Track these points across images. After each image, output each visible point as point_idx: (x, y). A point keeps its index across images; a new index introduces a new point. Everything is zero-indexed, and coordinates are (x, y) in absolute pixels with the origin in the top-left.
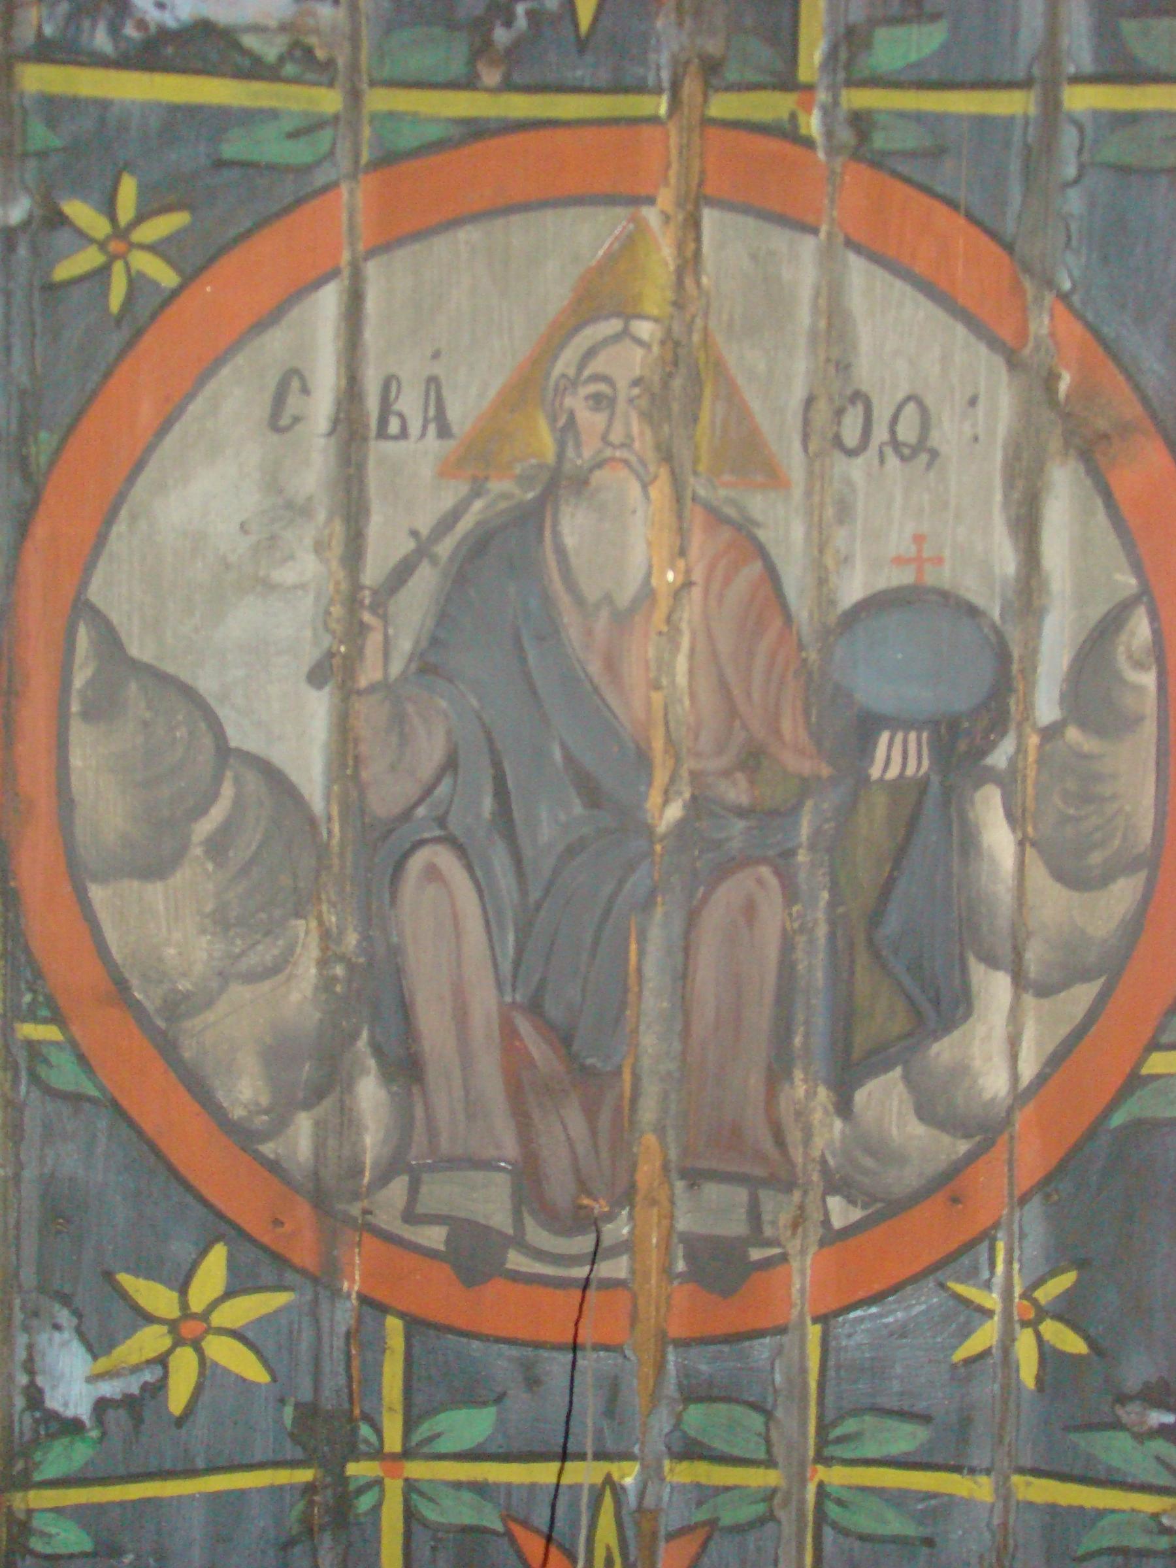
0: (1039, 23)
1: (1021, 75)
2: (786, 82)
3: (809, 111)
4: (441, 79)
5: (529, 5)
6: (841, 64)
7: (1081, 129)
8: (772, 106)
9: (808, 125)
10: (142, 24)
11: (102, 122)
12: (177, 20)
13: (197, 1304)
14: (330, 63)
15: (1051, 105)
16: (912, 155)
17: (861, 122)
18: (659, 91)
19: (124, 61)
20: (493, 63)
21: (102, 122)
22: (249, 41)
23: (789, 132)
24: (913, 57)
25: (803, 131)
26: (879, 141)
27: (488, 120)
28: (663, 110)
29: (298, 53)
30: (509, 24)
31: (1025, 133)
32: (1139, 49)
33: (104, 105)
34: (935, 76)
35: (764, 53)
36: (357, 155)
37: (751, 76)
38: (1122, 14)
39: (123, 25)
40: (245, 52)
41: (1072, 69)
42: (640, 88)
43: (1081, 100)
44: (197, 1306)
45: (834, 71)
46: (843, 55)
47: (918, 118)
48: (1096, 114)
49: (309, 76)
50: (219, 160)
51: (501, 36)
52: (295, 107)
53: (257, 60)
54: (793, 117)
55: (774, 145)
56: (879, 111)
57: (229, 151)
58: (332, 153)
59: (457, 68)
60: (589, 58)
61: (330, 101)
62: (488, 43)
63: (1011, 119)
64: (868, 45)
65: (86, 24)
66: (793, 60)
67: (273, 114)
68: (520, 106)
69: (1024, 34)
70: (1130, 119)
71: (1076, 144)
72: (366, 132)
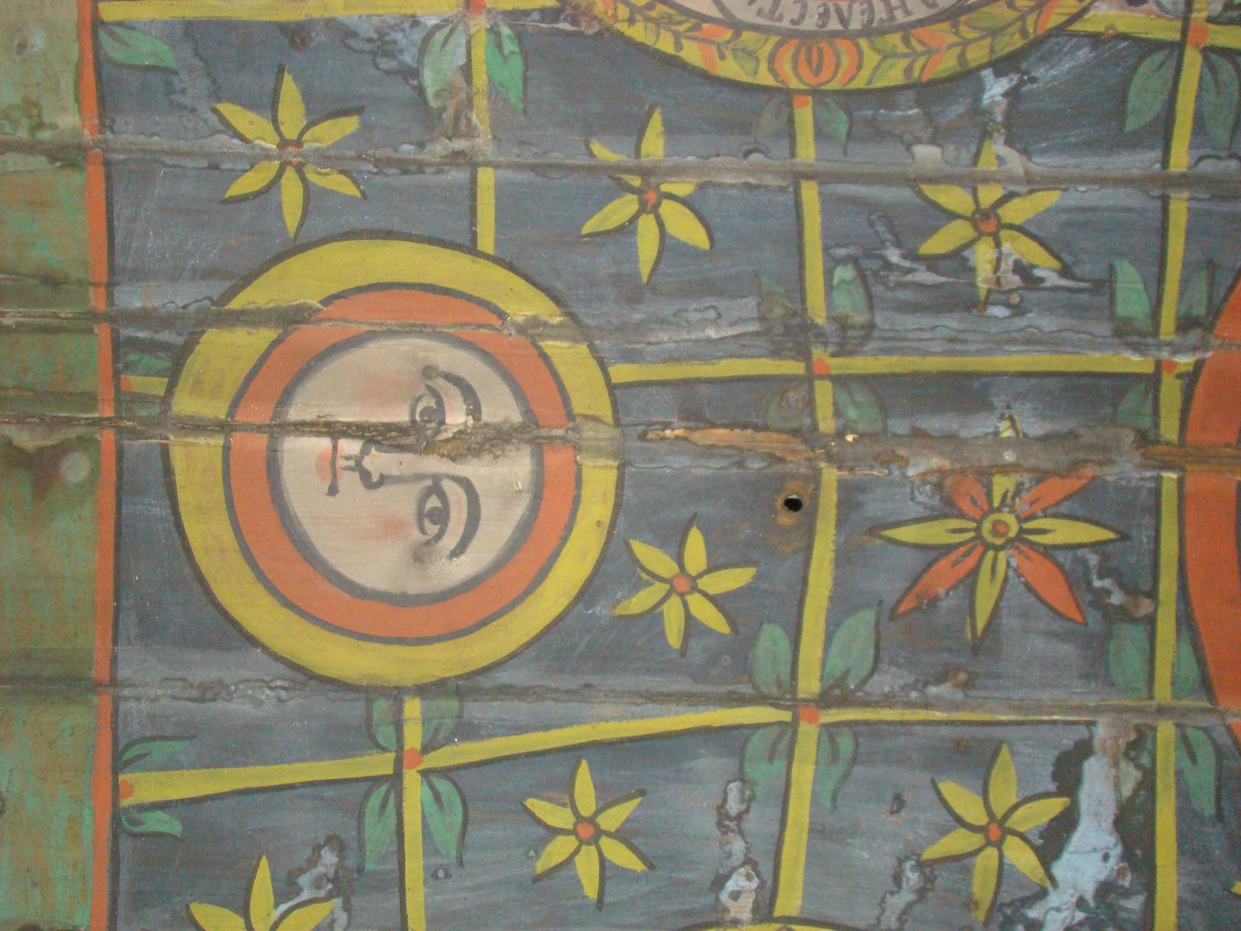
1: (1159, 204)
2: (1153, 381)
3: (1175, 365)
4: (1146, 645)
5: (1094, 577)
6: (1142, 340)
7: (1201, 159)
8: (1171, 391)
9: (1184, 365)
10: (1121, 873)
11: (1194, 906)
12: (1115, 845)
13: (605, 842)
14: (1138, 729)
15: (1182, 181)
16: (1212, 285)
17: (1186, 324)
18: (1158, 479)
19: (1150, 888)
20: (1136, 606)
21: (1194, 906)
22: (1127, 790)
23: (1191, 379)
24: (1140, 286)
25: (1191, 369)
26: (1200, 311)
27: (1178, 611)
28: (1173, 475)
29: (1133, 754)
30: (1108, 593)
32: (1148, 117)
33: (1181, 903)
34: (1155, 269)
35: (1131, 400)
36: (1204, 711)
37: (1148, 409)
38: (1121, 130)
39: (1122, 887)
40: (1135, 792)
41: (1158, 166)
42: (1157, 492)
43: (1180, 159)
45: (1146, 345)
46: (1135, 339)
47: (1185, 281)
49: (1149, 745)
50: (1217, 816)
51: (1116, 598)
52: (1172, 758)
53: (1140, 785)
54: (1179, 376)
55: (1200, 389)
56: (1178, 311)
57: (1209, 810)
58: (1205, 730)
59: (1139, 632)
60: (1134, 532)
61: (1166, 731)
62: (1121, 607)
63: (1189, 210)
64: (1128, 321)
65: (1122, 914)
66: (1138, 377)
67: (1179, 773)
68: (1168, 585)
69: (1129, 203)
71: (1210, 161)
72: (1187, 702)
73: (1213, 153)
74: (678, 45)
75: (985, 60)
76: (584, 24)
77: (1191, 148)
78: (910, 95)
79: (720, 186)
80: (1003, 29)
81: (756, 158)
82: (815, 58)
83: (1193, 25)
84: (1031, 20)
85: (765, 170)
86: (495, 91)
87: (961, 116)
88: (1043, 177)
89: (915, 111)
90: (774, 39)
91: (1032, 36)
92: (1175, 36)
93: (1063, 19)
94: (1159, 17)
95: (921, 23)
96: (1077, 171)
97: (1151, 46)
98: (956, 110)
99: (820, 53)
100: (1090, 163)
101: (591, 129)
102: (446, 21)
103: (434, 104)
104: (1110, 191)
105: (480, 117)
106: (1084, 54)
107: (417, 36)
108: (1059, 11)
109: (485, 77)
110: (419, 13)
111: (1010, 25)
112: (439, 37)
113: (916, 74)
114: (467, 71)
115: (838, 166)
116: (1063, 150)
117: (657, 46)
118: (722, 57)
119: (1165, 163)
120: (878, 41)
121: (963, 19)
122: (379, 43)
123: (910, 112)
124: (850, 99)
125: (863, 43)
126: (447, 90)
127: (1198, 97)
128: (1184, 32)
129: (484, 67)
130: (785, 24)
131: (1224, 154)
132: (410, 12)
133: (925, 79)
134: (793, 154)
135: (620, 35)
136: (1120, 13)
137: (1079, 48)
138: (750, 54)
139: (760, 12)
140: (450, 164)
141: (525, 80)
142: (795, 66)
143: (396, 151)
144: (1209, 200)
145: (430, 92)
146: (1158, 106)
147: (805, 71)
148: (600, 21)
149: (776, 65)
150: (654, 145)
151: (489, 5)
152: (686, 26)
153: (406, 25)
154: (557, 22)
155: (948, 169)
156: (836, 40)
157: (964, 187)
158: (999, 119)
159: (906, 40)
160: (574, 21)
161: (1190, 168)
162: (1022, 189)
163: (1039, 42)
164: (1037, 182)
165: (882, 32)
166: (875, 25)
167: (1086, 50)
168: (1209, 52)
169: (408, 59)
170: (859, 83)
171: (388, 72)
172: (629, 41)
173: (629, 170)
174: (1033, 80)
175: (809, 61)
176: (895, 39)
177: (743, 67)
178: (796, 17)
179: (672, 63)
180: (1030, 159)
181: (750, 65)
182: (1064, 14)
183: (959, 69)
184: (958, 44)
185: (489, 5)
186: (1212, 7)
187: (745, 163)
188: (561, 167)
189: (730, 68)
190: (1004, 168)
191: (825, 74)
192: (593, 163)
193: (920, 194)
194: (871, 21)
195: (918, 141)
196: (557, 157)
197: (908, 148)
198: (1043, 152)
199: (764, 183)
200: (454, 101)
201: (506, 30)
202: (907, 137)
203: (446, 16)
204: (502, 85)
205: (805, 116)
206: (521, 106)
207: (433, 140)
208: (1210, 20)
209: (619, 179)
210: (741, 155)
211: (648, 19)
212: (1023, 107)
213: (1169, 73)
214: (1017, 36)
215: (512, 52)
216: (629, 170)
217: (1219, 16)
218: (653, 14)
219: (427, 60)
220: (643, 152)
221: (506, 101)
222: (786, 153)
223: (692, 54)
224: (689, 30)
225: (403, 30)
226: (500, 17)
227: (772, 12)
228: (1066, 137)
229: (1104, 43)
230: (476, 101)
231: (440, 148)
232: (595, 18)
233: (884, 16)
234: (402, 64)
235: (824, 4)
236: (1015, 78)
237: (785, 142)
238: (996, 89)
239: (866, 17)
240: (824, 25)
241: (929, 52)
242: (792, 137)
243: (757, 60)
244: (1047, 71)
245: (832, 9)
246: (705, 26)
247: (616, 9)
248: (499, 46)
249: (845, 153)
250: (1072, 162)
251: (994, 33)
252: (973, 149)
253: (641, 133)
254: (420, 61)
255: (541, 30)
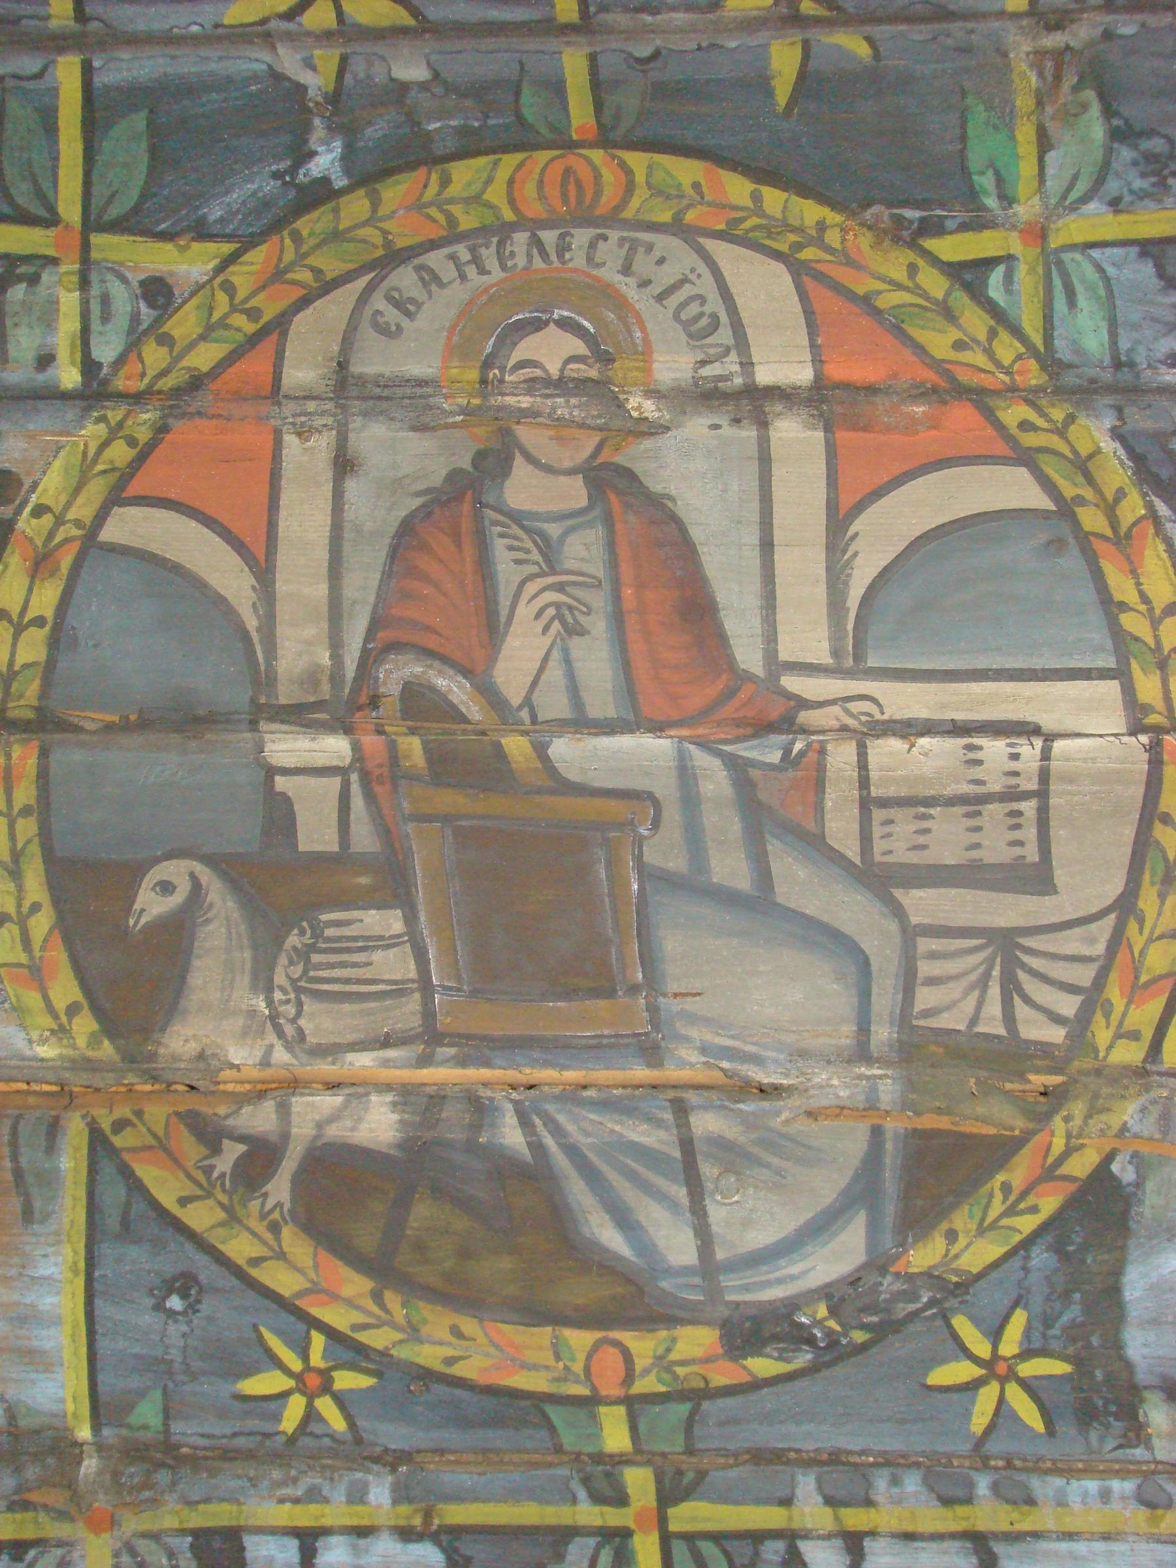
0: (141, 26)
1: (88, 10)
15: (60, 43)
31: (32, 17)
32: (119, 130)
38: (151, 111)
43: (67, 74)
44: (291, 1383)
48: (55, 92)
69: (129, 10)
70: (50, 128)
73: (25, 84)
74: (756, 198)
75: (343, 200)
76: (886, 218)
77: (56, 89)
78: (439, 149)
79: (689, 8)
80: (324, 242)
81: (643, 51)
82: (573, 192)
83: (76, 255)
84: (289, 256)
85: (631, 34)
86: (1006, 120)
87: (369, 123)
88: (251, 43)
89: (431, 127)
90: (628, 214)
91: (285, 233)
92: (96, 239)
93: (247, 257)
94: (122, 264)
95: (433, 245)
96: (203, 52)
97: (117, 226)
98: (376, 130)
99: (565, 196)
100: (188, 64)
101: (873, 79)
102: (1073, 208)
103: (1090, 95)
104: (156, 26)
105: (1026, 80)
106: (215, 213)
107: (1113, 186)
108: (254, 268)
109: (1020, 137)
110: (1110, 217)
111: (318, 246)
112: (1081, 187)
113: (434, 177)
114: (1044, 143)
115: (532, 44)
116: (228, 82)
117: (785, 195)
118: (696, 186)
119: (87, 70)
120: (489, 219)
121: (380, 252)
122: (1165, 172)
123: (438, 125)
124: (522, 140)
125: (508, 215)
126: (1072, 115)
127: (56, 159)
128: (86, 246)
129: (1021, 151)
130: (614, 235)
131: (10, 83)
132: (1123, 218)
133: (422, 171)
134: (593, 58)
135: (834, 205)
136: (173, 268)
137: (221, 220)
138: (658, 192)
139: (650, 248)
140: (1067, 12)
141: (963, 138)
142: (597, 176)
143: (1143, 25)
144: (20, 19)
145: (1095, 110)
146: (106, 145)
147: (585, 173)
148: (863, 224)
149: (624, 179)
150: (784, 60)
151: (1015, 234)
152: (748, 224)
153: (1127, 198)
154: (922, 220)
155: (380, 48)
156: (544, 216)
157: (355, 25)
158: (317, 122)
159: (452, 221)
160: (899, 220)
161: (54, 62)
162: (273, 25)
163: (277, 226)
164: (258, 35)
165: (483, 231)
166: (495, 240)
167: (212, 218)
168: (51, 220)
169: (1126, 154)
170: (510, 161)
171: (1151, 133)
172: (822, 199)
173: (817, 21)
174: (277, 175)
175: (579, 186)
176: (467, 222)
177: (668, 173)
178: (601, 244)
179: (765, 174)
180: (270, 66)
181: (659, 177)
182: (247, 264)
183: (378, 186)
184: (381, 220)
185: (1015, 234)
186: (56, 279)
187: (658, 42)
188: (909, 20)
189: (686, 171)
190: (304, 54)
191: (558, 168)
192: (868, 29)
193: (415, 13)
194: (501, 244)
195: (424, 86)
196: (919, 33)
197: (436, 75)
198: (255, 77)
199: (628, 16)
200: (1062, 101)
201: (991, 202)
202: (438, 90)
203: (1073, 216)
204: (996, 128)
205: (580, 114)
206: (970, 100)
207: (1092, 43)
208: (54, 261)
209: (830, 9)
210: (664, 52)
211: (800, 230)
212: (286, 139)
213: (99, 192)
214: (305, 233)
215: (982, 173)
216: (817, 21)
217: (44, 266)
218: (793, 237)
219: (1098, 155)
220: (799, 47)
221: (989, 108)
222: (601, 60)
223: (737, 188)
224: (742, 220)
225: (1131, 192)
226: (1000, 220)
227: (632, 250)
228: (225, 100)
229: (189, 229)
230: (1031, 102)
231: (1081, 33)
232: (870, 228)
233: (483, 251)
234: (1135, 147)
235: (564, 263)
236: (301, 178)
237: (604, 74)
238: (326, 161)
239: (508, 249)
240: (562, 237)
241: (418, 206)
242: (596, 85)
243: (649, 185)
244: (260, 188)
245: (554, 257)
246: (722, 227)
247: (844, 240)
248: (1000, 180)
249: (521, 63)
250: (213, 66)
251: (336, 236)
252: (348, 79)
253: (802, 75)
254: (1109, 152)
255: (942, 206)
